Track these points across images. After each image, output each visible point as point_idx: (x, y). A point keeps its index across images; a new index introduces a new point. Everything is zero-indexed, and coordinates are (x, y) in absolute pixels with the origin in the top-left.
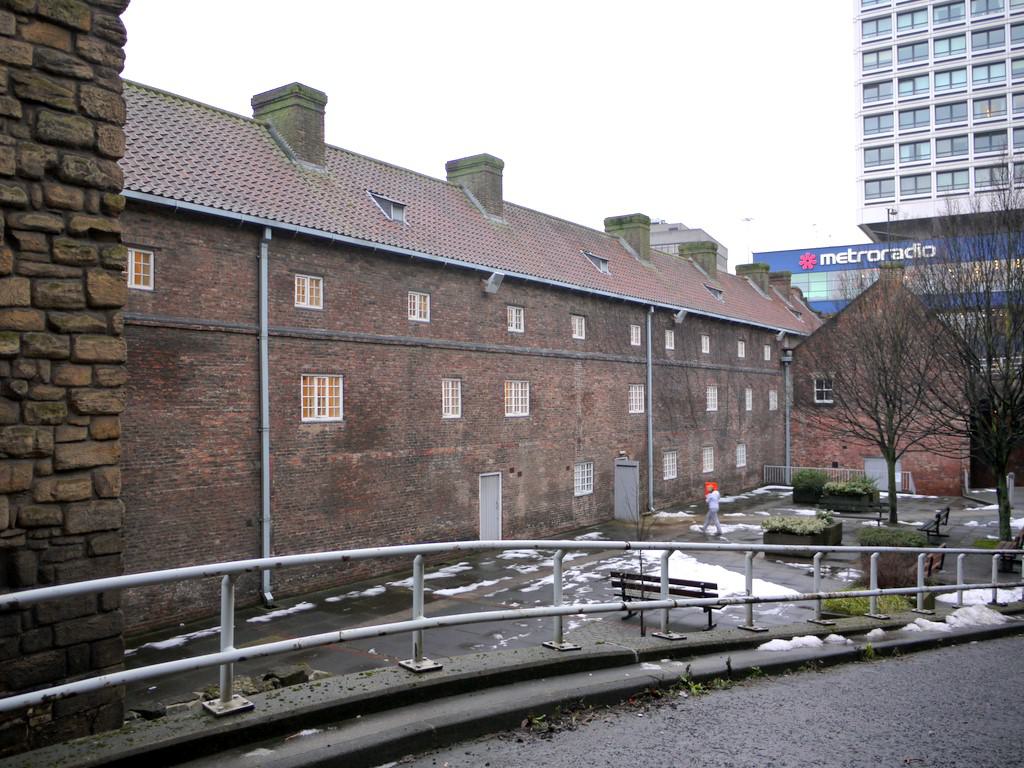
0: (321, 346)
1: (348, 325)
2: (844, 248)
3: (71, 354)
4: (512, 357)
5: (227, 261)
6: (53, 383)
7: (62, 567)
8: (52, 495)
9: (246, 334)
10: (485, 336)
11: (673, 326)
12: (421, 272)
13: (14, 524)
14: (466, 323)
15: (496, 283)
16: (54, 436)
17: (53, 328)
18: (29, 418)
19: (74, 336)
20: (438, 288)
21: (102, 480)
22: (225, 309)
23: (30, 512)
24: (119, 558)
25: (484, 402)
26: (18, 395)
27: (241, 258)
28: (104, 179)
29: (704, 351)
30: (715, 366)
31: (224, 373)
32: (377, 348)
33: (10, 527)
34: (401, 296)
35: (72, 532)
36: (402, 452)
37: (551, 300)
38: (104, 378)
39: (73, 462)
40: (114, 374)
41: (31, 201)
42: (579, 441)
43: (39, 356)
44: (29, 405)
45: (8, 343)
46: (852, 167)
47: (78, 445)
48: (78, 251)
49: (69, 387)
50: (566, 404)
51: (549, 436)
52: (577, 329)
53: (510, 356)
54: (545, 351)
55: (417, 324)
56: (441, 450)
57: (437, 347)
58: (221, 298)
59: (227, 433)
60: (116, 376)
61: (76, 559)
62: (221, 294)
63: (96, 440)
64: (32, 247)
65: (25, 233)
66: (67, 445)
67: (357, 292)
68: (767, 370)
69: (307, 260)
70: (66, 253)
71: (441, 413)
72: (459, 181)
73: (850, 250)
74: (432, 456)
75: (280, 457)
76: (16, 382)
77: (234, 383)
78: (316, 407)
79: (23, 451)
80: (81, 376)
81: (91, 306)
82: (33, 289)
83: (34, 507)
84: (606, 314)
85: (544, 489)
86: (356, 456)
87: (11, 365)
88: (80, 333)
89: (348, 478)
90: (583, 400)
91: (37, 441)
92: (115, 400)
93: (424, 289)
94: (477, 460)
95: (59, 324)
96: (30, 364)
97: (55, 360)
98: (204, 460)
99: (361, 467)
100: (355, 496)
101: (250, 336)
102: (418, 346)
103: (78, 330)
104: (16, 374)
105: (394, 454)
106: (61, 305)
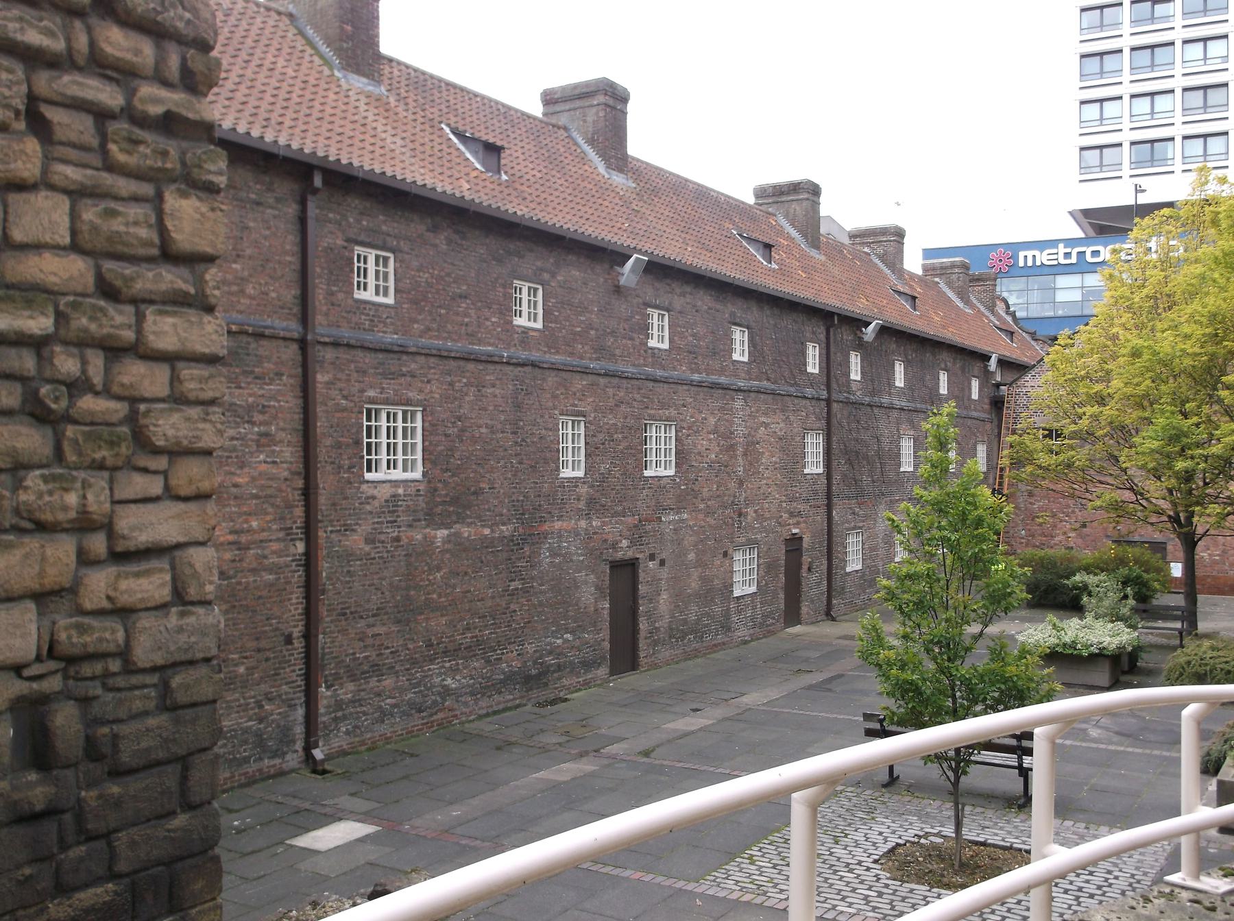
0: (392, 363)
1: (429, 329)
2: (1053, 243)
3: (137, 339)
4: (652, 386)
5: (255, 220)
6: (106, 392)
7: (124, 729)
8: (109, 598)
9: (284, 339)
10: (618, 352)
11: (860, 345)
12: (531, 251)
13: (45, 652)
14: (592, 332)
15: (633, 270)
16: (111, 489)
17: (108, 291)
18: (72, 457)
19: (143, 307)
20: (553, 275)
21: (188, 571)
22: (252, 298)
23: (69, 638)
24: (215, 710)
25: (617, 451)
26: (50, 411)
27: (275, 217)
28: (189, 22)
29: (897, 384)
30: (911, 405)
31: (251, 400)
32: (471, 366)
33: (39, 659)
34: (504, 286)
35: (140, 665)
36: (504, 528)
37: (704, 300)
38: (192, 385)
39: (143, 538)
40: (207, 380)
41: (70, 49)
42: (740, 515)
43: (82, 343)
44: (70, 431)
45: (35, 314)
46: (1065, 131)
47: (150, 506)
48: (148, 151)
49: (134, 401)
50: (724, 458)
51: (702, 506)
52: (737, 346)
53: (651, 384)
54: (696, 377)
55: (526, 331)
56: (557, 525)
57: (554, 368)
58: (248, 280)
59: (256, 497)
60: (211, 384)
61: (146, 713)
62: (246, 273)
63: (179, 498)
64: (73, 137)
65: (61, 110)
66: (133, 506)
67: (442, 278)
68: (975, 414)
69: (371, 225)
70: (129, 153)
71: (558, 469)
72: (563, 120)
73: (1061, 246)
74: (545, 535)
75: (333, 536)
76: (48, 387)
77: (266, 417)
78: (384, 456)
79: (61, 516)
80: (147, 379)
81: (169, 255)
82: (74, 215)
83: (80, 619)
84: (775, 325)
85: (694, 584)
86: (442, 533)
87: (39, 356)
88: (152, 302)
89: (430, 569)
90: (745, 454)
91: (84, 497)
92: (208, 426)
93: (535, 278)
94: (606, 541)
95: (118, 283)
96: (72, 355)
97: (114, 351)
98: (222, 539)
99: (447, 551)
100: (440, 596)
101: (288, 343)
102: (533, 371)
103: (147, 296)
104: (48, 373)
105: (492, 531)
106: (120, 248)
